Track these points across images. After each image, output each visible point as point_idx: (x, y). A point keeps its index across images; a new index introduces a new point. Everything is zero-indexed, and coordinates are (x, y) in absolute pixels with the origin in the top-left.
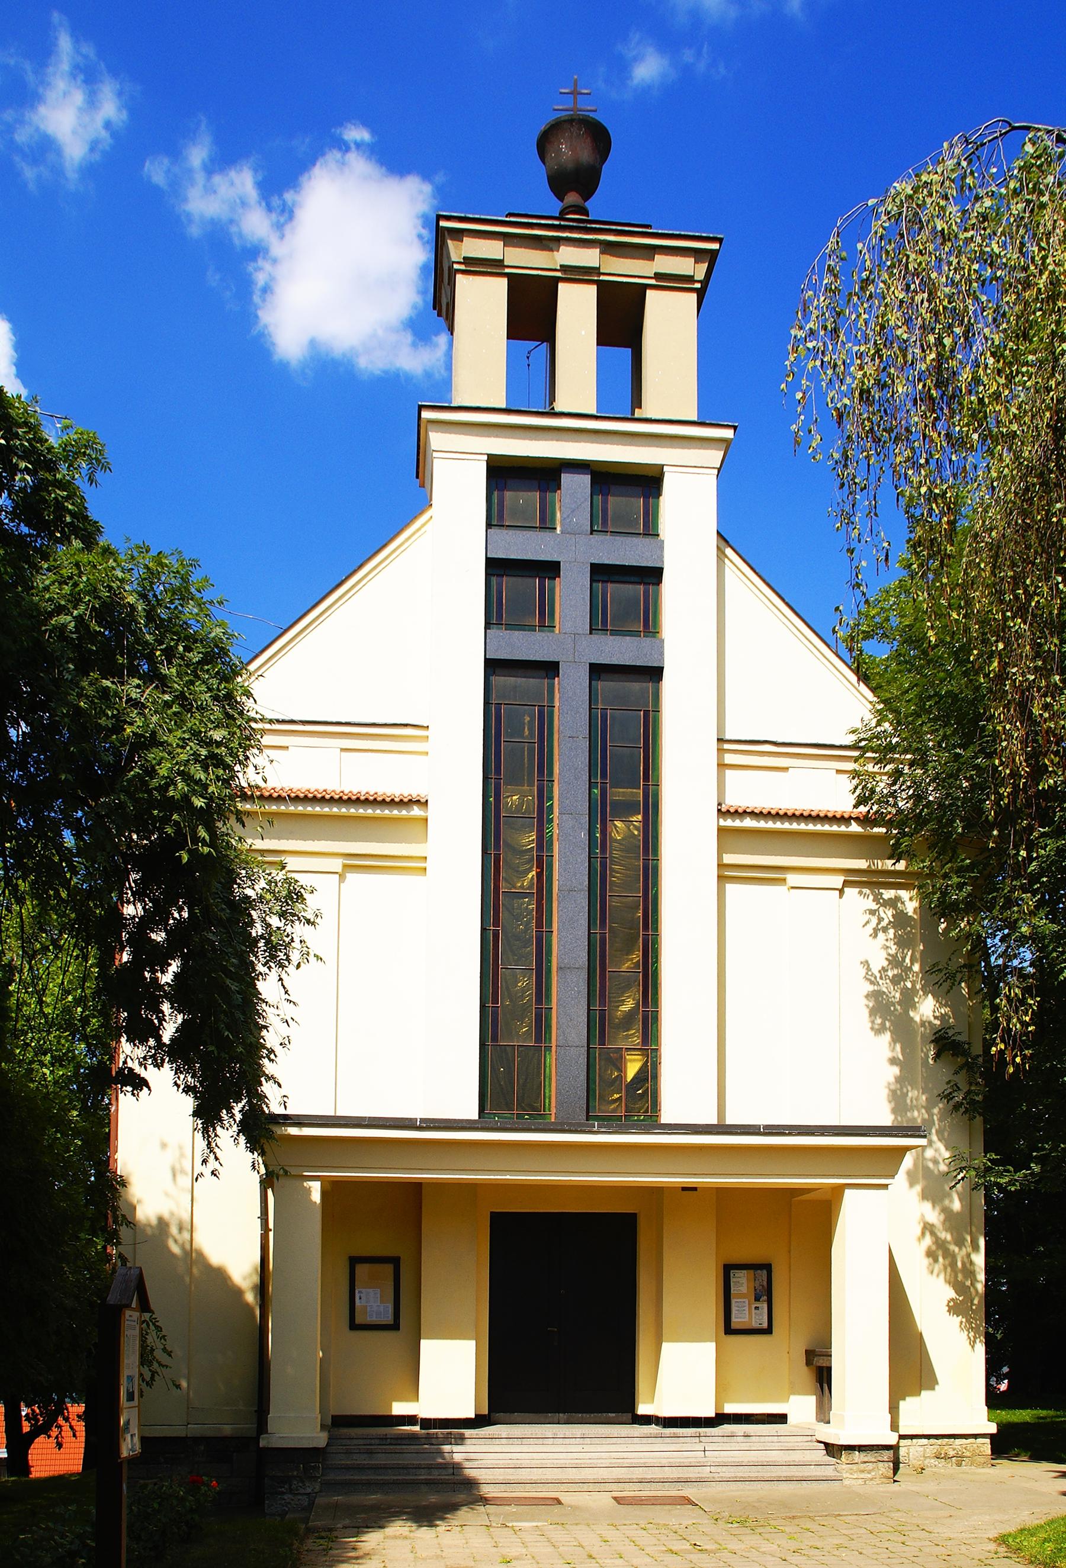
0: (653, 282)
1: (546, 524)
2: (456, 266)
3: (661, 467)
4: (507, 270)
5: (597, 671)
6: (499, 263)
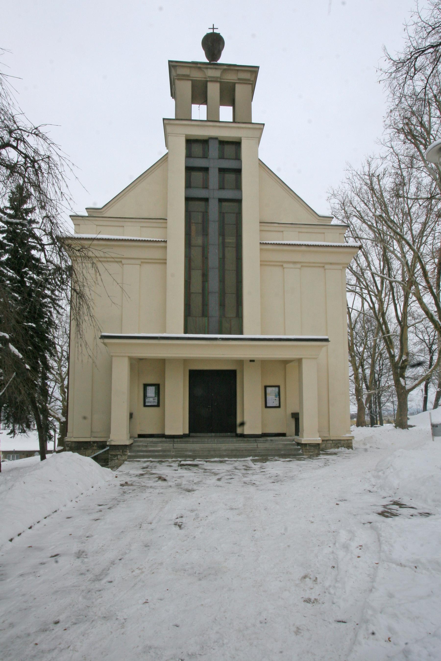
0: (237, 81)
1: (205, 156)
2: (175, 77)
3: (240, 139)
4: (192, 78)
5: (221, 200)
6: (188, 76)
